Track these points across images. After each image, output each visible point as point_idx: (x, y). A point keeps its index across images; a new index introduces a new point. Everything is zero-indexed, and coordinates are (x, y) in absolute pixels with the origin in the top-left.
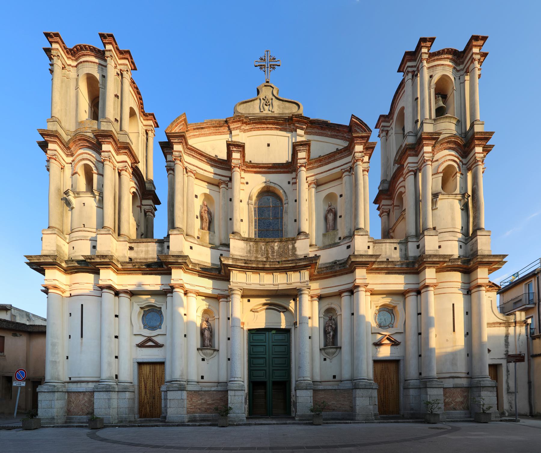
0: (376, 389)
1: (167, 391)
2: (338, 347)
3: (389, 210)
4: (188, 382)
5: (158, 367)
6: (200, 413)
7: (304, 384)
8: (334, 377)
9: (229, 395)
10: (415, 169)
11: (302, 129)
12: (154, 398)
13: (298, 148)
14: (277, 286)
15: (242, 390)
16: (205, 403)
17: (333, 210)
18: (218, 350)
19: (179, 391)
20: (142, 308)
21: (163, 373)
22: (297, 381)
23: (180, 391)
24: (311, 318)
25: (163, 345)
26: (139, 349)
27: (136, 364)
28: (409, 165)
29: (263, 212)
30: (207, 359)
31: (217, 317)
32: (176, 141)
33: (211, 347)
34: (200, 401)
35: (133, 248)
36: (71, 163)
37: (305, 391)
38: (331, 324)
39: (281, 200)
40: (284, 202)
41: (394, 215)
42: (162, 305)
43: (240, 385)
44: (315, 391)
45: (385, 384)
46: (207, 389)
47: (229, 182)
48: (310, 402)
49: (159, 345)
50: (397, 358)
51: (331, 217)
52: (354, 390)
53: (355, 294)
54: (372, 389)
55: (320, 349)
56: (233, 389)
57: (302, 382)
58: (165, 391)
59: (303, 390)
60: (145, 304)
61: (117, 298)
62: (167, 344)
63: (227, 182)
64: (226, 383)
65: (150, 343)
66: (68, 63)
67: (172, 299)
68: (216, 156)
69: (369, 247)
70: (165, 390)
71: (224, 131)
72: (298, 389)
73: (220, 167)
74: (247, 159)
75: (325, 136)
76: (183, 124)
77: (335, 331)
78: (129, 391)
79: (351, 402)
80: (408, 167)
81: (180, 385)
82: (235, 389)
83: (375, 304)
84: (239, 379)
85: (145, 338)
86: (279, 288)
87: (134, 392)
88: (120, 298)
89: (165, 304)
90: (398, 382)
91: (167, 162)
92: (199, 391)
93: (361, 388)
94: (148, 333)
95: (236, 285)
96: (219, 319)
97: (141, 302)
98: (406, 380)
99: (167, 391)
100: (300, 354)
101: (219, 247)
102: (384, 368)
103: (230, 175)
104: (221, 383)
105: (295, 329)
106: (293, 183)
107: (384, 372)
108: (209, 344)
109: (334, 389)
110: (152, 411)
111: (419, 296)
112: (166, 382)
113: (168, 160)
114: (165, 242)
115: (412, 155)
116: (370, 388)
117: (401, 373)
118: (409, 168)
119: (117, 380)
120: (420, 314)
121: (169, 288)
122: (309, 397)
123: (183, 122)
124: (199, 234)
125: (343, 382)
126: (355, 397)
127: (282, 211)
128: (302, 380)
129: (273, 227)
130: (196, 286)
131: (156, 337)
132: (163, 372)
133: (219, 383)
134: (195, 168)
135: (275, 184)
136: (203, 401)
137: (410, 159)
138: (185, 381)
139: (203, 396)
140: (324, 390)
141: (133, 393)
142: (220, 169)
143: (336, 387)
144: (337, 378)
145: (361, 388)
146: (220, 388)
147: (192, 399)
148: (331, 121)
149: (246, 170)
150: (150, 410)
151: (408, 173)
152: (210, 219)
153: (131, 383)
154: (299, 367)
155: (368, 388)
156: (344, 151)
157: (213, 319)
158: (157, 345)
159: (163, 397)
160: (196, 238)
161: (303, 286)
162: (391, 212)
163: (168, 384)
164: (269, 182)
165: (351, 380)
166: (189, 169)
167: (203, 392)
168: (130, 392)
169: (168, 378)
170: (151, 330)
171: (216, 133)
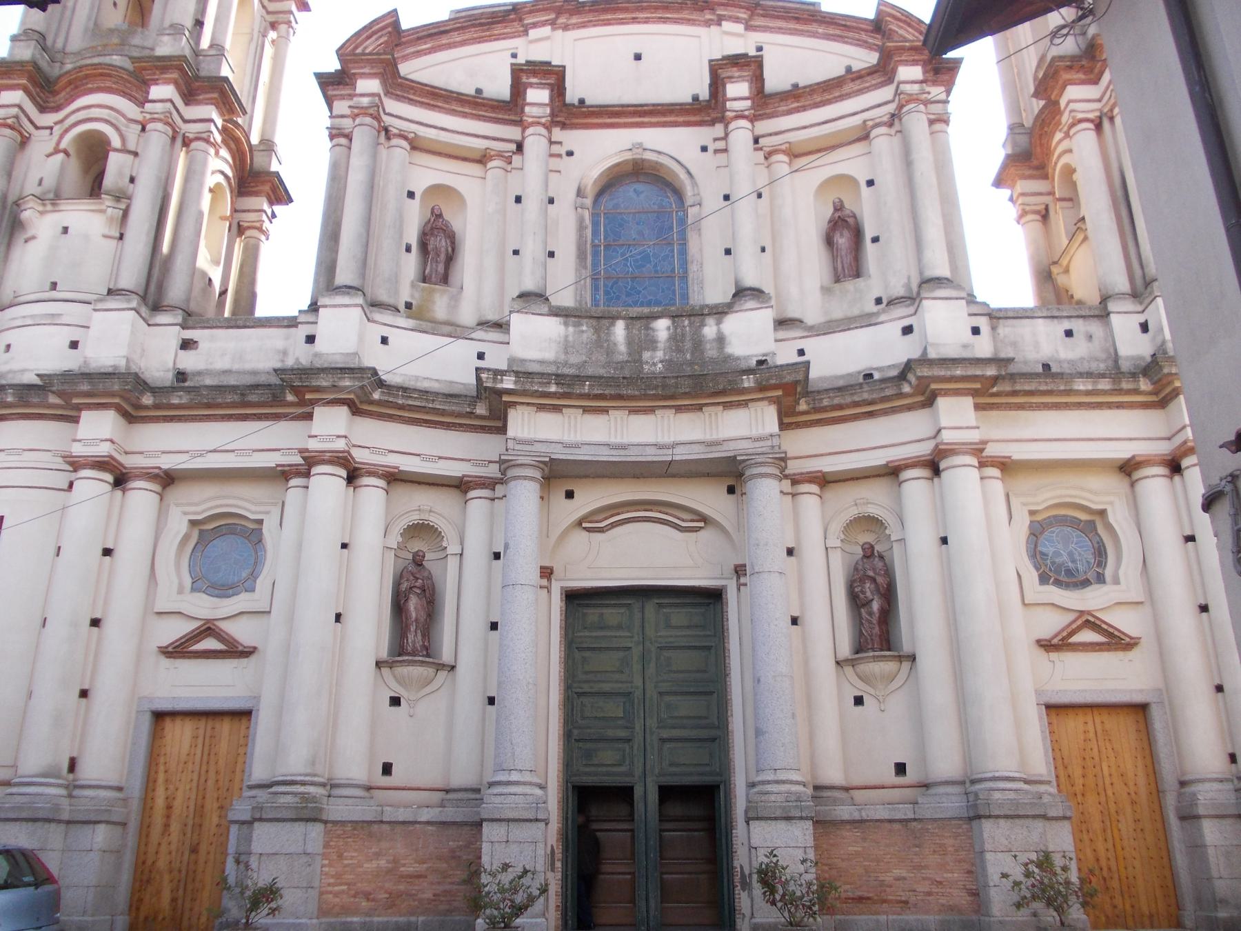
0: (1065, 818)
1: (250, 823)
2: (904, 656)
3: (1043, 207)
4: (333, 786)
5: (225, 726)
6: (367, 914)
7: (780, 798)
8: (901, 769)
9: (484, 838)
10: (1097, 117)
11: (737, 20)
12: (194, 850)
13: (723, 73)
14: (670, 452)
15: (537, 820)
16: (389, 871)
17: (851, 220)
18: (453, 668)
19: (296, 824)
20: (193, 523)
21: (241, 751)
22: (752, 785)
23: (302, 824)
24: (795, 552)
25: (255, 648)
26: (165, 662)
28: (1072, 106)
29: (621, 225)
30: (408, 700)
31: (453, 548)
32: (366, 70)
33: (428, 655)
34: (374, 864)
35: (196, 342)
36: (51, 128)
37: (782, 825)
38: (871, 573)
39: (678, 193)
40: (689, 200)
41: (1060, 220)
42: (267, 513)
43: (530, 799)
44: (823, 825)
45: (1103, 799)
46: (402, 815)
47: (514, 153)
49: (240, 648)
50: (1138, 698)
51: (842, 240)
52: (975, 823)
53: (944, 475)
54: (1044, 817)
55: (838, 663)
57: (769, 788)
58: (244, 823)
59: (774, 823)
61: (119, 493)
62: (271, 650)
63: (511, 154)
64: (478, 791)
65: (210, 644)
66: (187, 117)
67: (306, 495)
68: (479, 91)
69: (976, 331)
70: (247, 817)
71: (505, 31)
72: (758, 819)
73: (490, 117)
74: (572, 96)
76: (389, 33)
77: (889, 594)
78: (108, 822)
79: (969, 872)
80: (1071, 111)
81: (305, 798)
82: (511, 815)
83: (1024, 504)
84: (527, 777)
85: (193, 625)
86: (677, 458)
87: (124, 825)
88: (130, 494)
89: (276, 511)
90: (1157, 792)
91: (331, 117)
93: (998, 817)
94: (204, 607)
95: (528, 448)
96: (461, 555)
97: (196, 504)
98: (1183, 784)
99: (250, 823)
100: (759, 681)
101: (473, 329)
102: (1091, 735)
103: (519, 138)
104: (455, 790)
105: (739, 589)
106: (716, 151)
107: (1096, 750)
108: (418, 646)
109: (900, 821)
110: (180, 902)
112: (251, 787)
113: (335, 113)
114: (300, 323)
115: (1077, 81)
116: (1035, 817)
117: (1162, 755)
118: (1073, 114)
119: (71, 776)
121: (300, 461)
123: (390, 29)
124: (412, 296)
125: (932, 791)
126: (982, 852)
127: (683, 222)
128: (769, 782)
129: (655, 266)
131: (232, 620)
132: (244, 744)
133: (447, 791)
134: (413, 127)
135: (659, 153)
136: (383, 863)
137: (1073, 92)
138: (323, 785)
139: (384, 845)
140: (860, 822)
141: (119, 829)
142: (489, 121)
143: (905, 812)
144: (912, 775)
145: (998, 817)
146: (450, 814)
147: (340, 856)
149: (568, 122)
150: (174, 900)
151: (1073, 125)
152: (450, 249)
153: (120, 789)
154: (759, 732)
155: (1027, 817)
156: (869, 74)
157: (442, 555)
158: (236, 651)
159: (232, 848)
160: (402, 307)
161: (760, 450)
162: (1052, 212)
163: (262, 795)
164: (640, 150)
165: (963, 783)
166: (395, 131)
167: (386, 827)
169: (259, 771)
170: (217, 596)
171: (480, 38)
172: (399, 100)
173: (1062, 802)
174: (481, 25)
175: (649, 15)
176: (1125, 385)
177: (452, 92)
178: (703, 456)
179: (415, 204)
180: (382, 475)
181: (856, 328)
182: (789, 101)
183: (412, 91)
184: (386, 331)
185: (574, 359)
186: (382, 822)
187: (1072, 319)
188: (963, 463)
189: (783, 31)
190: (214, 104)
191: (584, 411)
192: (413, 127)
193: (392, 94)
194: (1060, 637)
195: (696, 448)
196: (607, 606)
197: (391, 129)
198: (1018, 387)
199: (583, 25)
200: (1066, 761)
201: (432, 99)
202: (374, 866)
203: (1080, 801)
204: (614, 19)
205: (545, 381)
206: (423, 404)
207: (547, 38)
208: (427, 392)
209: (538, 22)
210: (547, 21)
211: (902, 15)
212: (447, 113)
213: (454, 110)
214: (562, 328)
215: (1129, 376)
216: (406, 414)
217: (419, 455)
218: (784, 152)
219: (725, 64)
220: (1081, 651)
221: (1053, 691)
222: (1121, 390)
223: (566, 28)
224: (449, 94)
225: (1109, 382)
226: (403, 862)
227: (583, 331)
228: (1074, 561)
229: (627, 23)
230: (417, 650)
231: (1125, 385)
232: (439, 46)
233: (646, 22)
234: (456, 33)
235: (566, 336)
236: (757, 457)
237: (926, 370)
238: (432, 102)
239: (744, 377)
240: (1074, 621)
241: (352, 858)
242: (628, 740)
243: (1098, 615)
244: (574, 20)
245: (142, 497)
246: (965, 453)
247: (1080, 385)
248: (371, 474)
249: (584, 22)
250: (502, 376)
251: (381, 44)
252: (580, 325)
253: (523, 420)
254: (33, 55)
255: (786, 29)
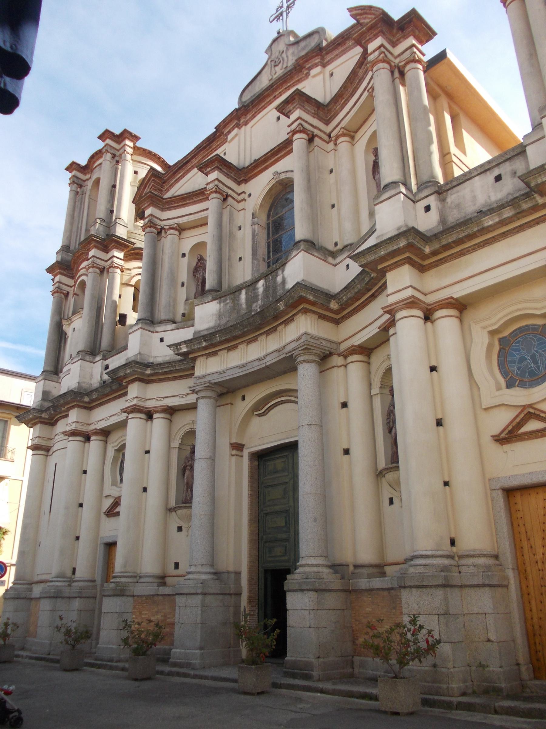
4: (140, 577)
11: (316, 65)
20: (492, 333)
27: (500, 492)
32: (146, 205)
48: (308, 625)
56: (184, 592)
60: (120, 442)
61: (429, 324)
75: (349, 50)
84: (199, 569)
92: (153, 595)
97: (116, 441)
111: (87, 444)
120: (148, 452)
122: (307, 612)
124: (185, 309)
130: (110, 417)
134: (176, 221)
135: (286, 172)
145: (410, 587)
147: (141, 613)
148: (180, 159)
155: (431, 587)
167: (160, 598)
168: (83, 597)
172: (170, 210)
173: (483, 572)
174: (205, 147)
175: (281, 90)
176: (525, 206)
177: (189, 193)
178: (277, 359)
179: (186, 259)
180: (161, 411)
181: (368, 238)
182: (340, 101)
183: (173, 203)
184: (161, 335)
185: (223, 322)
186: (158, 595)
187: (501, 165)
188: (402, 316)
189: (339, 56)
190: (115, 248)
191: (207, 356)
192: (176, 221)
193: (165, 209)
194: (507, 431)
195: (275, 355)
196: (277, 458)
197: (165, 227)
198: (444, 243)
199: (254, 117)
200: (529, 534)
201: (184, 201)
202: (156, 618)
203: (540, 568)
204: (266, 104)
205: (199, 341)
206: (171, 369)
207: (236, 135)
208: (170, 362)
209: (230, 130)
210: (234, 125)
211: (361, 10)
212: (193, 205)
213: (195, 201)
214: (218, 305)
215: (524, 197)
216: (170, 376)
217: (177, 396)
218: (344, 135)
219: (283, 106)
220: (528, 439)
221: (506, 477)
222: (523, 211)
223: (246, 124)
224: (188, 195)
225: (510, 209)
226: (168, 616)
227: (227, 303)
228: (535, 362)
229: (273, 102)
230: (188, 500)
231: (525, 206)
232: (187, 171)
233: (280, 96)
234: (194, 159)
235: (220, 310)
236: (295, 352)
237: (362, 260)
238: (184, 203)
239: (279, 304)
240: (517, 416)
241: (146, 614)
242: (287, 540)
243: (539, 406)
244: (249, 116)
245: (95, 444)
246: (401, 309)
247: (489, 221)
248: (157, 412)
249: (253, 115)
250: (180, 346)
251: (151, 187)
252: (226, 300)
253: (200, 364)
254: (62, 257)
255: (340, 53)
